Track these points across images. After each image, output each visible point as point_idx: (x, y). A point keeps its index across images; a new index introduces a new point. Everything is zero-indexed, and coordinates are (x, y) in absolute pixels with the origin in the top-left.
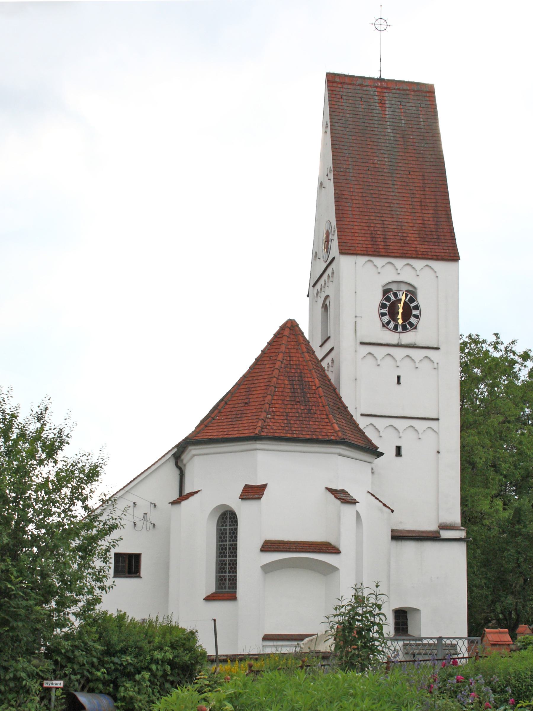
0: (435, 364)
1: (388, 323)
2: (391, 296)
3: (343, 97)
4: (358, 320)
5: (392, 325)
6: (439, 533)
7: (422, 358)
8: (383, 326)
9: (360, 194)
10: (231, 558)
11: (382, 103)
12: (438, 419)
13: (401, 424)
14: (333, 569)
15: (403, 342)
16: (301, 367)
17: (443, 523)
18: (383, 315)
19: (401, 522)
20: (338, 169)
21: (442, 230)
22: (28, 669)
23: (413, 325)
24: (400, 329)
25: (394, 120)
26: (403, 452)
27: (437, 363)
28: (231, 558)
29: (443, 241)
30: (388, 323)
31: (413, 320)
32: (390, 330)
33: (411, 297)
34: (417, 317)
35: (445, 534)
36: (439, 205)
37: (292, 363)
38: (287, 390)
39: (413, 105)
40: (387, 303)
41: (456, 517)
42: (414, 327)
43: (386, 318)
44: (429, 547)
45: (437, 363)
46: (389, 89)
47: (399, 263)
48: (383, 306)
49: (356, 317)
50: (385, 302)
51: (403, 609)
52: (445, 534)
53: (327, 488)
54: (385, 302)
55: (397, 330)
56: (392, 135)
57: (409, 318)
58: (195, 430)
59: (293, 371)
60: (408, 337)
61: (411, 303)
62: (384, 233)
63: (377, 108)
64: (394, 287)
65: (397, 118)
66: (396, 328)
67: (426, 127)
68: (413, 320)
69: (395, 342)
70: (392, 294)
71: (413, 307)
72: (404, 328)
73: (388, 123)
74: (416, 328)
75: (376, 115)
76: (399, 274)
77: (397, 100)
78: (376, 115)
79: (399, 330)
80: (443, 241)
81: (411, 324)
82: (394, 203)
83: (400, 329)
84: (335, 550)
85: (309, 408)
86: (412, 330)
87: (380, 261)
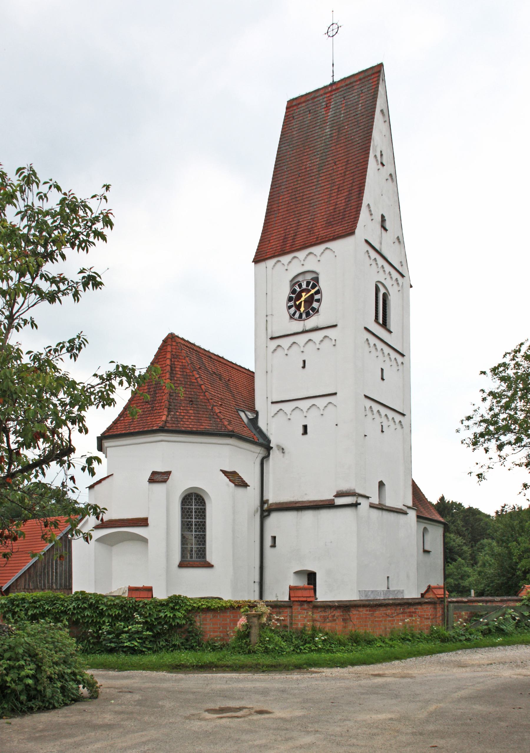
0: (334, 341)
3: (333, 164)
4: (269, 318)
6: (333, 500)
7: (322, 339)
8: (291, 318)
10: (197, 533)
12: (335, 394)
13: (304, 405)
14: (145, 540)
15: (307, 329)
17: (340, 491)
18: (290, 307)
19: (306, 494)
22: (490, 571)
23: (315, 309)
24: (304, 316)
27: (335, 340)
28: (197, 533)
31: (315, 305)
32: (296, 320)
33: (313, 283)
34: (318, 301)
35: (339, 501)
42: (316, 311)
44: (325, 514)
45: (335, 340)
47: (301, 254)
49: (267, 316)
50: (291, 295)
52: (339, 501)
53: (221, 470)
57: (312, 303)
66: (301, 316)
68: (315, 305)
69: (300, 330)
71: (300, 288)
72: (308, 315)
74: (318, 311)
76: (303, 265)
81: (313, 309)
83: (304, 316)
84: (143, 522)
87: (285, 259)
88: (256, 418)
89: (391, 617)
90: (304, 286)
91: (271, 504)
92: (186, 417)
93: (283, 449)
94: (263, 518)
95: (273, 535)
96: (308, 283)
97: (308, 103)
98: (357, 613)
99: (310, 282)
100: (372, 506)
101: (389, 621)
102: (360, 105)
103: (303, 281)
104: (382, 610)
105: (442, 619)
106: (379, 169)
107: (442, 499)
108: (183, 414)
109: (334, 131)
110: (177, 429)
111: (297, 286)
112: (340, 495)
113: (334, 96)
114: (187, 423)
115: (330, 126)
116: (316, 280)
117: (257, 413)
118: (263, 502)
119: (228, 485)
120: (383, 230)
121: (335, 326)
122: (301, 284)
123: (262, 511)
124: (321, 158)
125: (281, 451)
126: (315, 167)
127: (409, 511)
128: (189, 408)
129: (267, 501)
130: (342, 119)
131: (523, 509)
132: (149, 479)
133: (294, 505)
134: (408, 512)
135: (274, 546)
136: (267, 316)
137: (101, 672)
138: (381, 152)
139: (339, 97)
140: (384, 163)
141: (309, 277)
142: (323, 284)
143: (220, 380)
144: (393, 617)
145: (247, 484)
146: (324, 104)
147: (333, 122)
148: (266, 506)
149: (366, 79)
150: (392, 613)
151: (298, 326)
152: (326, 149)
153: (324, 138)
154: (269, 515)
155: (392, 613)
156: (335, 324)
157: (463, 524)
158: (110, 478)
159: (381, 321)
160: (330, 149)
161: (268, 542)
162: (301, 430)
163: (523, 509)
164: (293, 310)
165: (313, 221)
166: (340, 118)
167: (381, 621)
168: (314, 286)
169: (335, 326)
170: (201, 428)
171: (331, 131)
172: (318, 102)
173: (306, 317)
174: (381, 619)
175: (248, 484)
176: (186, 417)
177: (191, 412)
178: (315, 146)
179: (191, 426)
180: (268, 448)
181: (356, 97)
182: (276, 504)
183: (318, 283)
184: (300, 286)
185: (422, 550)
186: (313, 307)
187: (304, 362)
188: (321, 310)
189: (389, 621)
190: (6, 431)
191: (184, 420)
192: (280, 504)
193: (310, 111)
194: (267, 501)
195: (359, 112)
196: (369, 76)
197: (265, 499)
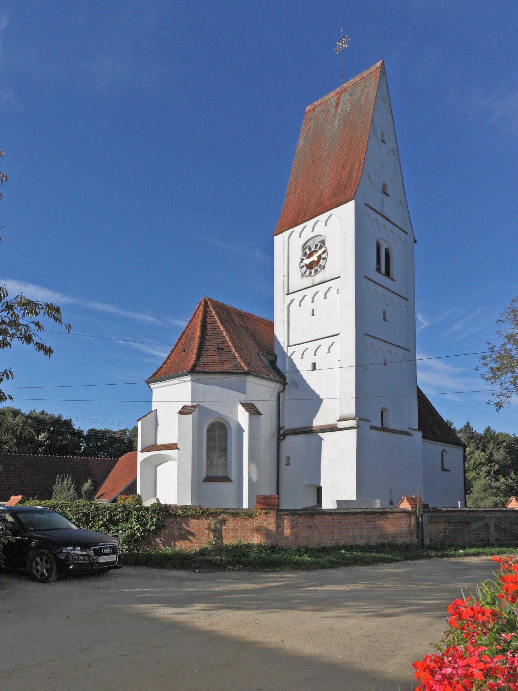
23: (322, 266)
33: (321, 245)
34: (324, 259)
35: (341, 425)
52: (341, 425)
60: (318, 278)
66: (310, 273)
71: (310, 251)
74: (324, 268)
88: (275, 360)
89: (360, 525)
90: (313, 249)
91: (286, 430)
92: (212, 361)
93: (296, 384)
94: (279, 441)
95: (288, 455)
96: (316, 246)
97: (322, 105)
98: (323, 520)
100: (372, 428)
101: (358, 529)
102: (363, 97)
104: (350, 518)
105: (417, 528)
106: (380, 146)
107: (488, 430)
108: (209, 359)
109: (341, 122)
110: (204, 370)
111: (308, 250)
112: (341, 420)
113: (342, 95)
114: (211, 366)
115: (338, 119)
116: (323, 242)
117: (276, 356)
118: (279, 429)
120: (384, 195)
121: (339, 277)
122: (311, 247)
123: (279, 435)
124: (330, 145)
126: (325, 153)
127: (413, 432)
128: (214, 354)
129: (283, 428)
130: (348, 111)
132: (179, 412)
133: (305, 430)
134: (412, 434)
135: (288, 464)
136: (284, 277)
137: (306, 574)
138: (382, 132)
139: (347, 95)
140: (385, 141)
141: (317, 240)
142: (328, 245)
143: (247, 331)
144: (362, 525)
145: (260, 413)
146: (335, 103)
147: (341, 115)
148: (282, 432)
149: (369, 77)
150: (361, 522)
151: (308, 281)
153: (333, 129)
154: (284, 438)
155: (361, 522)
156: (338, 276)
159: (383, 270)
160: (338, 137)
161: (283, 461)
162: (310, 367)
166: (347, 111)
167: (350, 529)
168: (321, 247)
169: (339, 277)
170: (224, 369)
171: (339, 123)
172: (330, 103)
173: (315, 273)
174: (349, 527)
175: (262, 413)
176: (212, 361)
177: (216, 357)
179: (214, 368)
180: (284, 384)
181: (360, 92)
182: (291, 430)
183: (324, 244)
184: (310, 249)
185: (440, 469)
187: (313, 310)
188: (327, 266)
189: (358, 529)
191: (210, 363)
192: (293, 429)
193: (323, 112)
194: (283, 428)
195: (362, 103)
196: (371, 73)
197: (281, 426)
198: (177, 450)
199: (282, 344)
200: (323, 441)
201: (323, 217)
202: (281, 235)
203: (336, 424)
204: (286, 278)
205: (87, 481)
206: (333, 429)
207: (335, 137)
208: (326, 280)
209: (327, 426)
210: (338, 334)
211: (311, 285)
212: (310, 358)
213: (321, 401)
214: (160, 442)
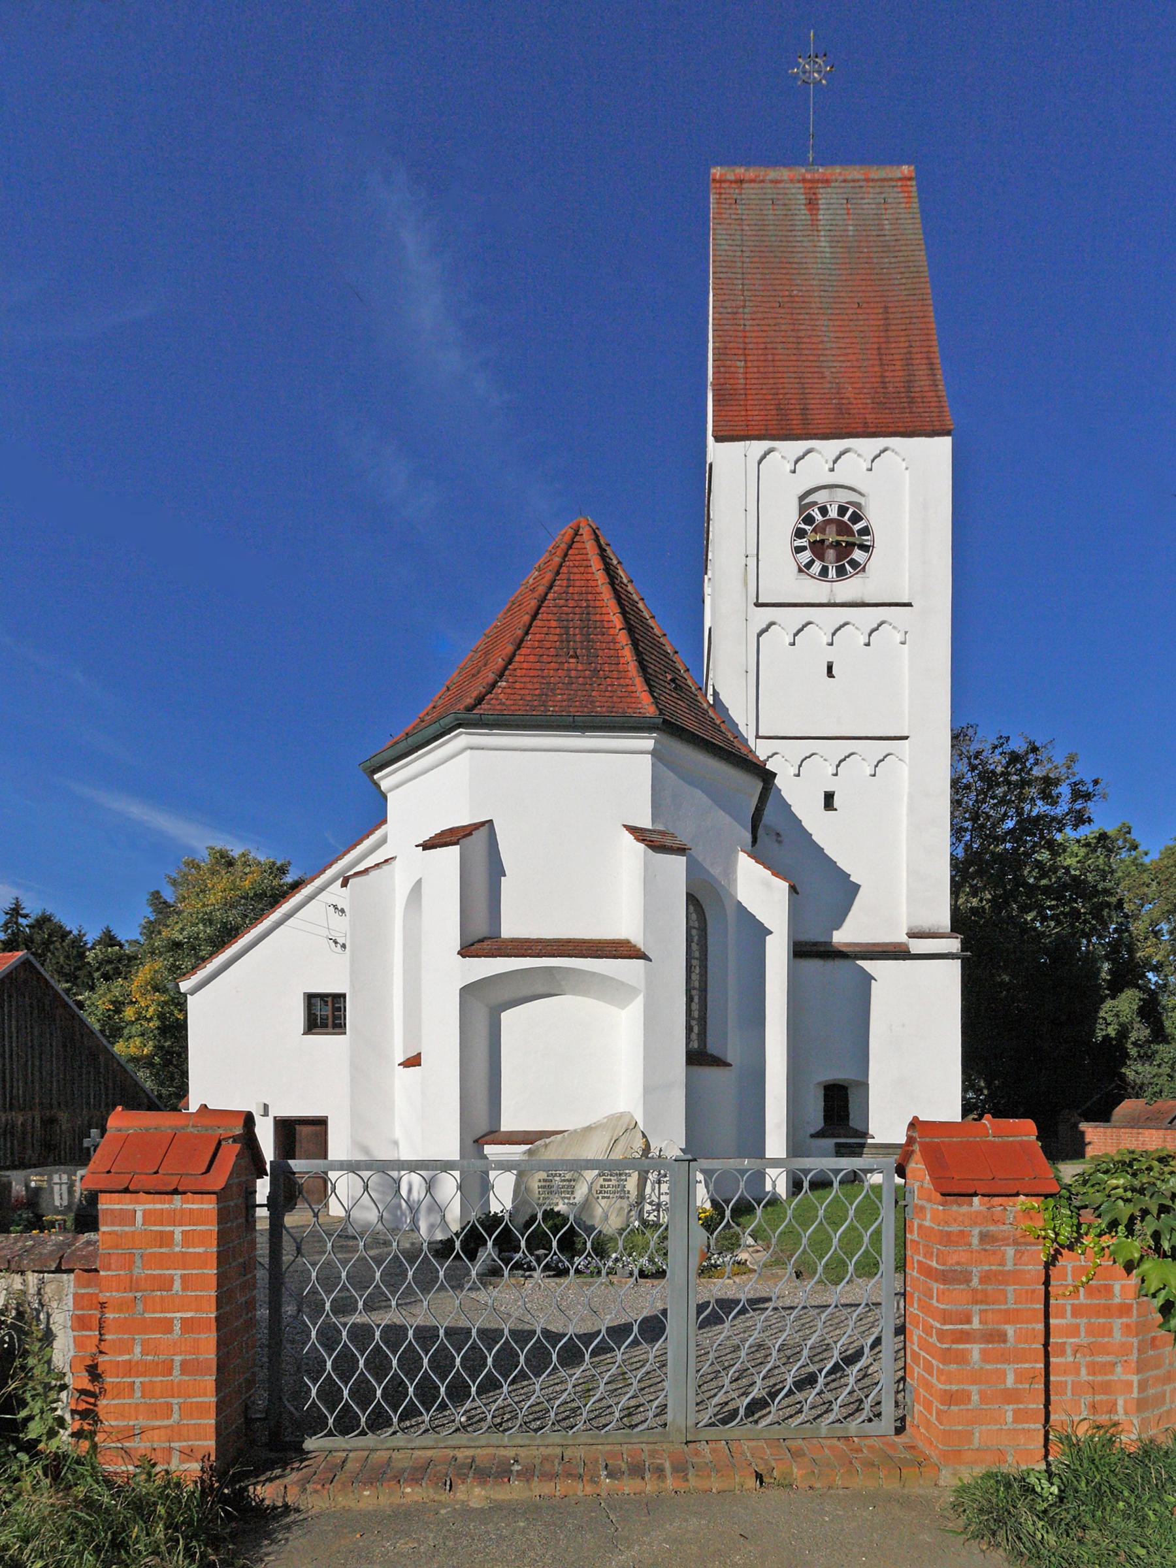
1: (809, 565)
2: (814, 514)
5: (817, 567)
8: (800, 570)
9: (763, 346)
11: (812, 204)
16: (590, 597)
17: (916, 927)
18: (799, 550)
20: (722, 310)
21: (918, 389)
24: (832, 573)
25: (831, 228)
26: (837, 802)
29: (921, 405)
30: (809, 565)
31: (858, 555)
34: (865, 548)
35: (917, 946)
36: (914, 350)
37: (571, 590)
38: (551, 637)
39: (871, 201)
40: (807, 527)
41: (943, 920)
43: (806, 556)
46: (827, 181)
48: (800, 533)
50: (803, 526)
51: (840, 1083)
52: (917, 946)
54: (803, 526)
55: (827, 576)
56: (828, 250)
58: (733, 897)
59: (571, 603)
60: (847, 589)
61: (854, 523)
62: (802, 401)
63: (803, 212)
64: (821, 497)
65: (840, 223)
67: (894, 232)
70: (816, 510)
71: (858, 531)
72: (841, 571)
73: (822, 233)
74: (864, 569)
75: (798, 223)
77: (840, 196)
78: (798, 223)
79: (830, 576)
80: (921, 405)
81: (854, 564)
82: (826, 355)
83: (832, 573)
85: (596, 668)
86: (857, 573)
90: (833, 513)
93: (778, 834)
99: (848, 509)
103: (831, 503)
119: (768, 885)
125: (774, 837)
131: (851, 879)
133: (814, 949)
141: (843, 497)
151: (817, 590)
152: (828, 280)
157: (81, 1496)
158: (386, 867)
163: (851, 879)
164: (806, 556)
165: (781, 420)
169: (909, 605)
178: (795, 247)
186: (852, 560)
190: (1171, 933)
198: (642, 961)
199: (742, 728)
200: (873, 981)
201: (871, 444)
202: (742, 443)
203: (906, 945)
204: (752, 562)
205: (1125, 1074)
206: (898, 953)
207: (828, 280)
208: (867, 601)
209: (874, 944)
210: (906, 738)
211: (825, 601)
212: (820, 777)
213: (856, 888)
214: (509, 930)
